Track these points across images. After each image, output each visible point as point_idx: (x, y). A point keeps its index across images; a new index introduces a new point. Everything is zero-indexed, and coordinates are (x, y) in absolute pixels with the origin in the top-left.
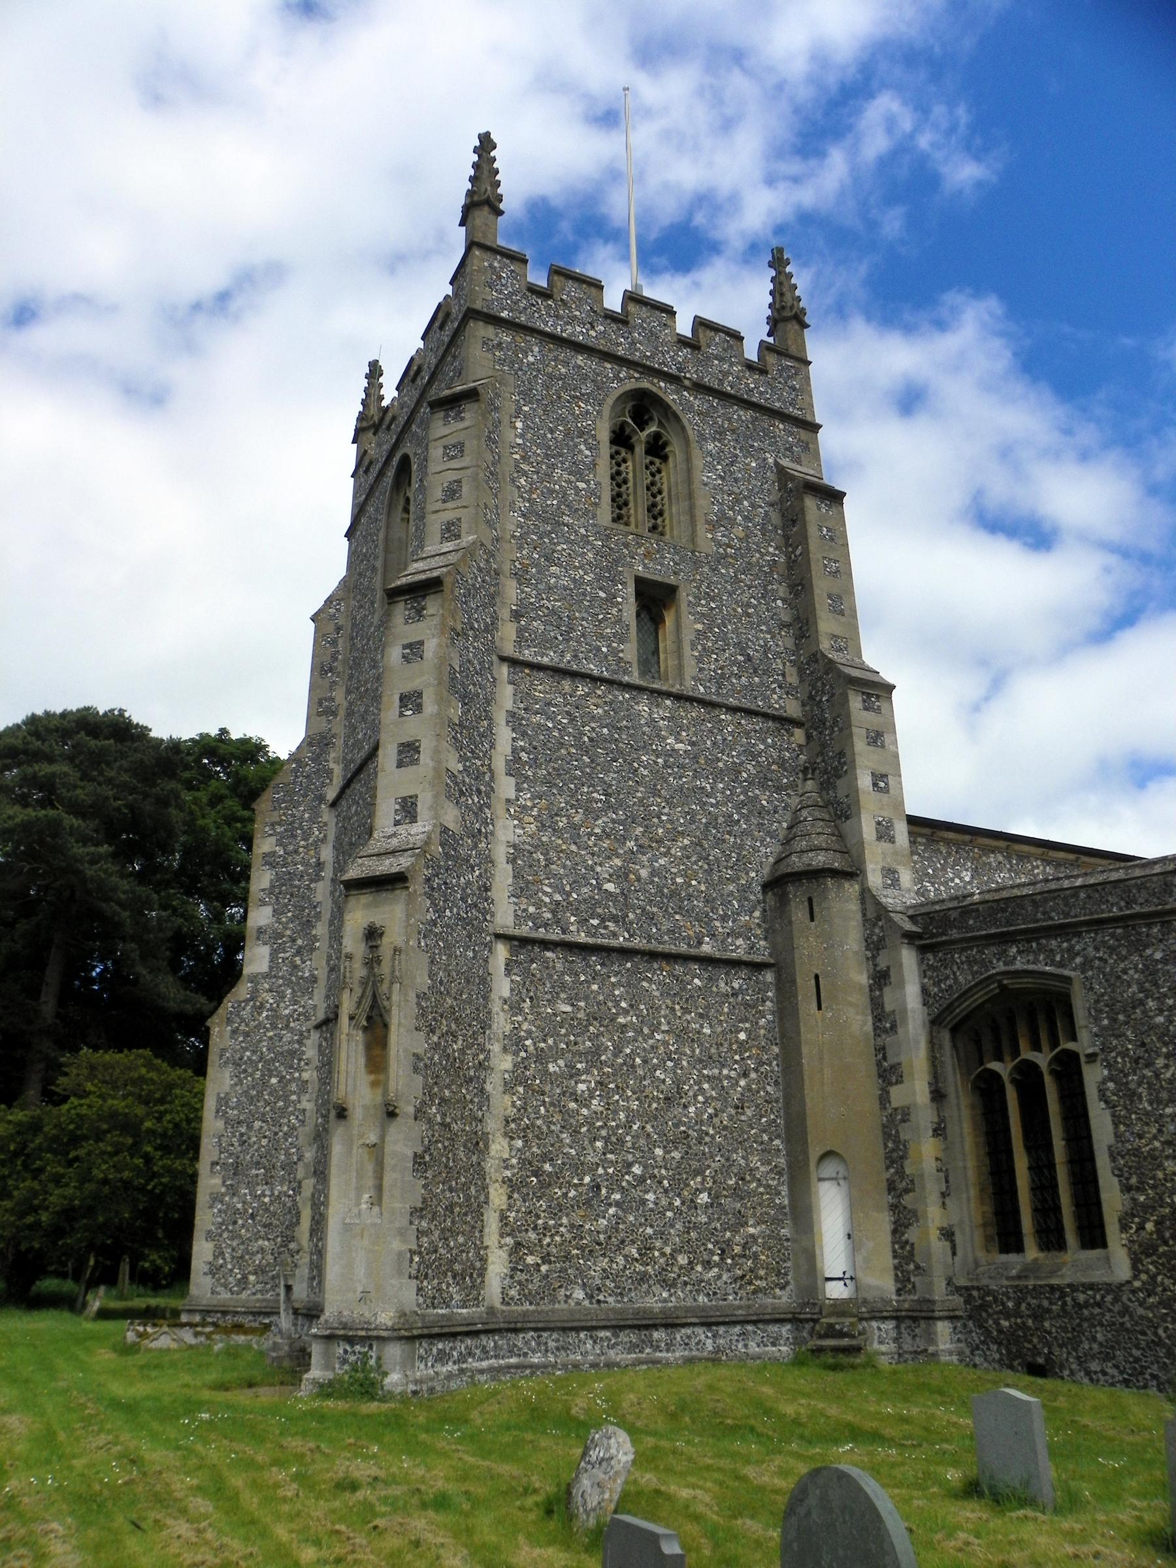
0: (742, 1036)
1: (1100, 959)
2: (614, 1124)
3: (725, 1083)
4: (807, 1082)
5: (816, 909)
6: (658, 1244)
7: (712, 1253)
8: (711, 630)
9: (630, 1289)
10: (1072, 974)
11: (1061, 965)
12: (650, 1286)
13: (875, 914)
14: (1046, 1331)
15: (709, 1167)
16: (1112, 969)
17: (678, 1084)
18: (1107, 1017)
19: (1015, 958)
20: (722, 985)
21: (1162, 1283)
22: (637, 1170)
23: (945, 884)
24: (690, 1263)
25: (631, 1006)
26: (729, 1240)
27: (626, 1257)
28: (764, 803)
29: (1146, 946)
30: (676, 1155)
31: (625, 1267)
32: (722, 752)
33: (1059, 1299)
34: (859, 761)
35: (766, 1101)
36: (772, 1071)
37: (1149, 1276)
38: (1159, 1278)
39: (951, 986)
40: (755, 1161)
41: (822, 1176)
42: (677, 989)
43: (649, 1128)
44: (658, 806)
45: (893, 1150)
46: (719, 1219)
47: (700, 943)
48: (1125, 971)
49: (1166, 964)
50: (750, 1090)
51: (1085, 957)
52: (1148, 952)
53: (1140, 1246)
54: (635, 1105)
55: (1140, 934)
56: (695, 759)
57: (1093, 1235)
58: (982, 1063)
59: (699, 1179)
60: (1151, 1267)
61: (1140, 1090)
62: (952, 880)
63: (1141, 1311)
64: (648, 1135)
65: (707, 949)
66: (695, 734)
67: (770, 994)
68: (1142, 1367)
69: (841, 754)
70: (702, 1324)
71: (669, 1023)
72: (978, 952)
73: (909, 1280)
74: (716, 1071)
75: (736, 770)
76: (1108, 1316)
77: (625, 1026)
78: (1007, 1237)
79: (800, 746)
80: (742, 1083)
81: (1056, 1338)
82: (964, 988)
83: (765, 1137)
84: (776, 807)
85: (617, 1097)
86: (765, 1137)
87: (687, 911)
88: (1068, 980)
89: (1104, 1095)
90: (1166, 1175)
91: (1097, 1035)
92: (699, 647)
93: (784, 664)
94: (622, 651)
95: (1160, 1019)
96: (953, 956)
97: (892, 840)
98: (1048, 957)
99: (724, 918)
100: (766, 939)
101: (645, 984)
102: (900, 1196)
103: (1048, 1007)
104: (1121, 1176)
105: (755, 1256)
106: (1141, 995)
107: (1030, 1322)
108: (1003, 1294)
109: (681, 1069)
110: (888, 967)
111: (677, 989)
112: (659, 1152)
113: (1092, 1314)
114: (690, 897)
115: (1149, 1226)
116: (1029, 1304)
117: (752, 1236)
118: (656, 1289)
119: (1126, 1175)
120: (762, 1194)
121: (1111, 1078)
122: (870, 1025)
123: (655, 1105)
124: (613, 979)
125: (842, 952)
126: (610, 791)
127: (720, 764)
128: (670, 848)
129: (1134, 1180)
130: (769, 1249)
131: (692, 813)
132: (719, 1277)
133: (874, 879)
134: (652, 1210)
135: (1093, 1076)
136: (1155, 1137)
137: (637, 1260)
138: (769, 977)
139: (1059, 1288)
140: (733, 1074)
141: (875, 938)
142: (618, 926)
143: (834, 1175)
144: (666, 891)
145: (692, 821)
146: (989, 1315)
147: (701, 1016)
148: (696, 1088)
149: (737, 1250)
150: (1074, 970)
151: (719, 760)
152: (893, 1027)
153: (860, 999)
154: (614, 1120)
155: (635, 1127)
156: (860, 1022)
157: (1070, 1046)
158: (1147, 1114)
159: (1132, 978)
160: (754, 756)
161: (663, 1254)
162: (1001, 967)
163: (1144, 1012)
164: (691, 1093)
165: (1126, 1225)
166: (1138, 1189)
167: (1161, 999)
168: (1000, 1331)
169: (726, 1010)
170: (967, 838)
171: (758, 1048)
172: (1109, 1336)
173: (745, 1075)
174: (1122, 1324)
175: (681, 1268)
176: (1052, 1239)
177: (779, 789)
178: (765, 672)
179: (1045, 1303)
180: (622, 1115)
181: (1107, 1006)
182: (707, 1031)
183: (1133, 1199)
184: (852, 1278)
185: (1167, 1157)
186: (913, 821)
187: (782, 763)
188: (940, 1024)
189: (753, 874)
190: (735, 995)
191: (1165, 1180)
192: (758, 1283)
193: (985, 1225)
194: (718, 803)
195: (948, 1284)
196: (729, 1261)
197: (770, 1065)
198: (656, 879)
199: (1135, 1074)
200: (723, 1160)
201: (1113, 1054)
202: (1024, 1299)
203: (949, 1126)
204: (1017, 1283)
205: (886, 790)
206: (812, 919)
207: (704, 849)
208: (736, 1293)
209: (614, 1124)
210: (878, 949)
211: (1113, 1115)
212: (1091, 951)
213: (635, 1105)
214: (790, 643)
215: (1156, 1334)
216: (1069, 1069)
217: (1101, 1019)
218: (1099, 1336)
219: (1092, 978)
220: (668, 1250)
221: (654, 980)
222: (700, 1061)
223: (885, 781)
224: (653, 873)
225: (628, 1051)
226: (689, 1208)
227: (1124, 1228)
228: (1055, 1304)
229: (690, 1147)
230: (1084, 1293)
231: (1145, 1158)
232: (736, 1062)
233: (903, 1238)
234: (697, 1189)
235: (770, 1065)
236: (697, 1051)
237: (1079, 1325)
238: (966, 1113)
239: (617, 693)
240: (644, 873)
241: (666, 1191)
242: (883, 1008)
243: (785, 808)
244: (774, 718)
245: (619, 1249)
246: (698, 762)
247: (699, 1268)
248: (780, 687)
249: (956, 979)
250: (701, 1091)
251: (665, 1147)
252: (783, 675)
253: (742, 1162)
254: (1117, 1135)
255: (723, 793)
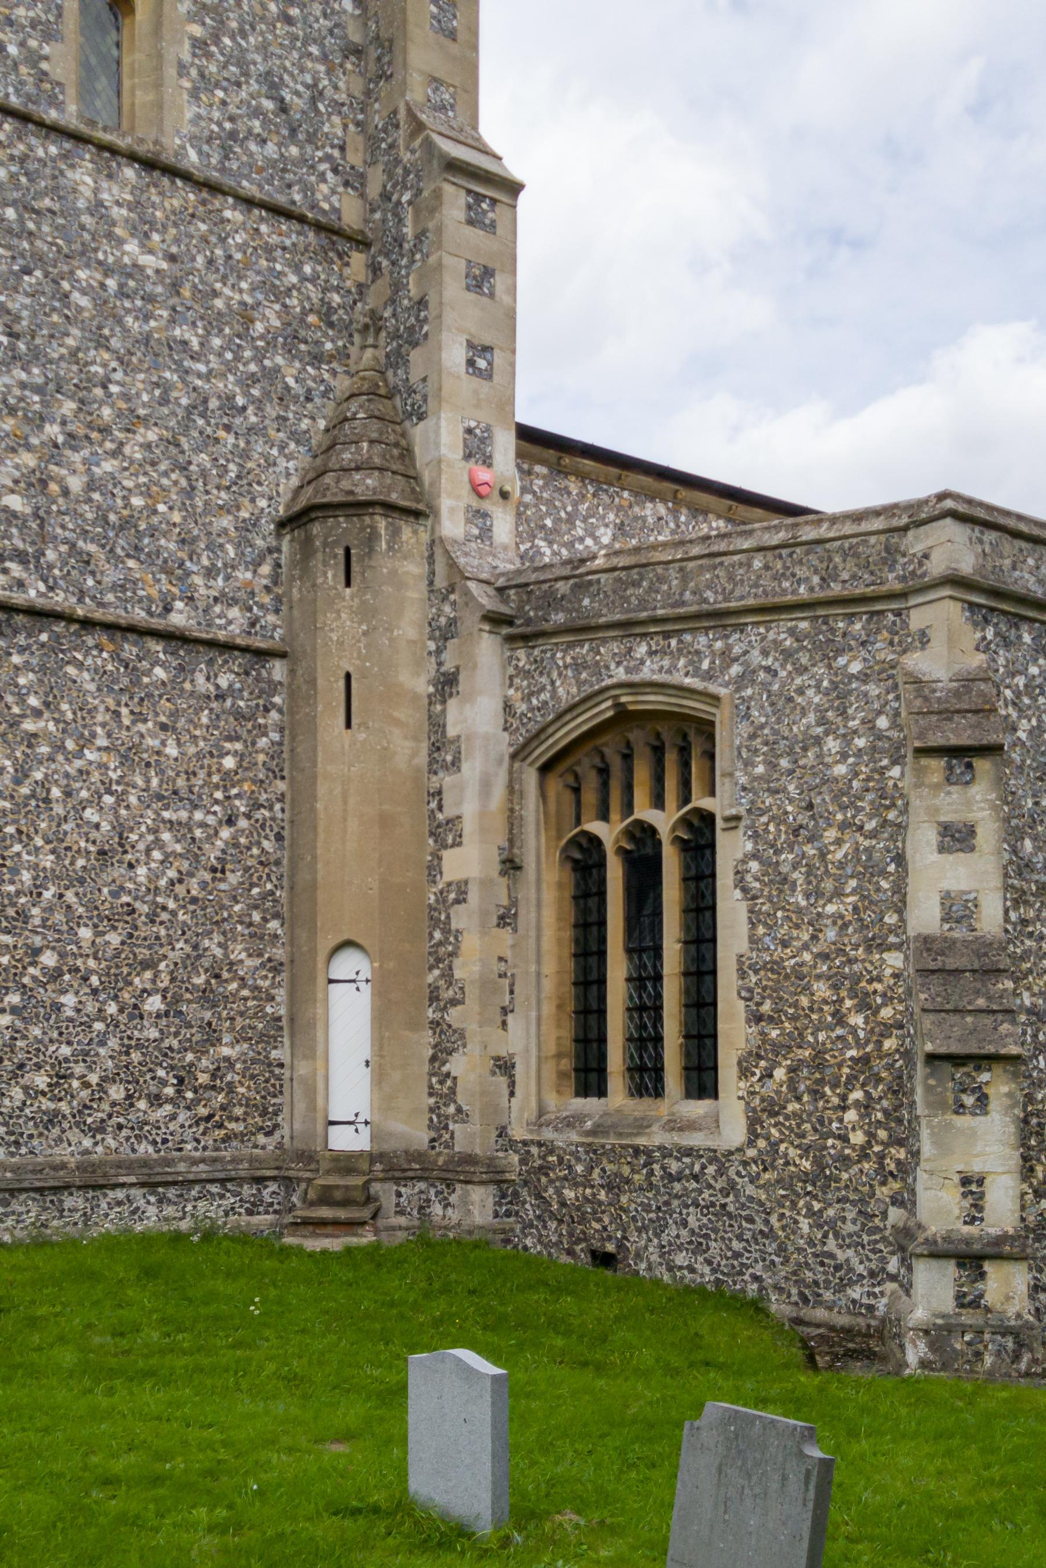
0: (229, 763)
1: (768, 669)
2: (11, 889)
3: (198, 833)
4: (321, 836)
5: (355, 567)
6: (79, 1069)
7: (164, 1083)
8: (217, 40)
9: (31, 1136)
10: (723, 692)
11: (709, 676)
12: (63, 1131)
13: (448, 581)
14: (621, 1208)
15: (165, 957)
16: (783, 685)
17: (121, 831)
18: (764, 762)
19: (642, 662)
20: (200, 679)
21: (786, 1155)
22: (49, 959)
23: (570, 545)
24: (129, 1097)
25: (47, 704)
26: (191, 1065)
27: (26, 1089)
28: (291, 381)
29: (840, 652)
30: (114, 939)
31: (24, 1103)
32: (224, 280)
33: (644, 1166)
34: (450, 317)
35: (261, 863)
36: (273, 819)
37: (770, 1144)
38: (783, 1147)
39: (546, 703)
40: (238, 952)
41: (332, 977)
42: (125, 681)
43: (70, 897)
44: (105, 365)
45: (440, 944)
46: (176, 1034)
47: (168, 609)
48: (801, 691)
49: (865, 682)
50: (236, 845)
51: (746, 664)
52: (842, 661)
53: (763, 1100)
54: (48, 861)
55: (833, 630)
56: (175, 287)
57: (702, 1081)
58: (578, 821)
59: (148, 975)
60: (773, 1131)
61: (795, 875)
62: (581, 540)
63: (750, 1190)
64: (69, 907)
65: (180, 618)
66: (177, 241)
67: (277, 700)
68: (742, 1264)
69: (422, 303)
70: (142, 1185)
71: (109, 735)
72: (591, 649)
73: (446, 1127)
74: (184, 815)
75: (246, 315)
76: (706, 1194)
77: (35, 735)
78: (589, 1078)
79: (360, 286)
80: (225, 833)
81: (634, 1218)
82: (564, 705)
83: (256, 917)
84: (309, 391)
85: (17, 848)
86: (256, 917)
87: (149, 555)
88: (715, 699)
89: (742, 880)
90: (813, 1002)
91: (744, 789)
92: (194, 72)
93: (345, 127)
94: (46, 58)
95: (841, 770)
96: (553, 656)
97: (488, 461)
98: (691, 662)
99: (210, 573)
100: (277, 611)
101: (71, 670)
102: (444, 1009)
103: (679, 738)
104: (749, 999)
105: (231, 1088)
106: (819, 730)
107: (602, 1195)
108: (571, 1154)
109: (128, 807)
110: (458, 668)
111: (125, 681)
112: (85, 933)
113: (685, 1189)
114: (153, 532)
115: (780, 1074)
116: (603, 1170)
117: (227, 1059)
118: (74, 1135)
119: (757, 998)
120: (246, 999)
121: (755, 856)
122: (439, 752)
123: (81, 862)
124: (16, 659)
125: (390, 639)
126: (17, 328)
127: (219, 303)
128: (121, 444)
129: (767, 1007)
130: (253, 1077)
131: (167, 388)
132: (173, 1117)
133: (452, 524)
134: (70, 1020)
135: (731, 849)
136: (806, 947)
137: (43, 1093)
138: (278, 670)
139: (648, 1152)
140: (211, 820)
141: (443, 620)
142: (27, 569)
143: (353, 977)
144: (112, 517)
145: (164, 401)
146: (551, 1181)
147: (164, 727)
148: (150, 838)
149: (203, 1078)
150: (726, 685)
151: (215, 294)
152: (456, 763)
153: (410, 715)
154: (12, 882)
155: (47, 895)
156: (408, 751)
157: (705, 803)
158: (799, 911)
159: (810, 703)
160: (279, 294)
161: (86, 1085)
162: (620, 674)
163: (820, 756)
164: (141, 846)
165: (747, 1069)
166: (771, 1019)
167: (847, 738)
168: (563, 1204)
169: (205, 720)
170: (614, 471)
171: (254, 782)
172: (705, 1220)
173: (230, 822)
174: (724, 1206)
175: (114, 1104)
176: (647, 1079)
177: (317, 359)
178: (311, 138)
179: (626, 1170)
180: (26, 876)
181: (766, 743)
182: (172, 750)
183: (762, 1033)
184: (366, 1123)
185: (819, 977)
186: (527, 435)
187: (326, 313)
188: (524, 760)
189: (263, 503)
190: (220, 697)
191: (811, 1009)
192: (232, 1126)
193: (559, 1056)
194: (210, 371)
195: (500, 1136)
196: (189, 1095)
197: (271, 808)
198: (96, 496)
199: (792, 851)
200: (188, 949)
201: (764, 819)
202: (598, 1162)
203: (522, 912)
204: (589, 1140)
205: (487, 375)
206: (348, 584)
207: (183, 452)
208: (198, 1141)
209: (11, 889)
210: (446, 639)
211: (751, 911)
212: (756, 657)
213: (48, 861)
214: (358, 87)
215: (767, 1222)
216: (699, 837)
217: (754, 765)
218: (691, 1220)
219: (751, 698)
220: (94, 1079)
221: (88, 666)
222: (160, 797)
223: (488, 358)
224: (91, 486)
225: (38, 776)
226: (131, 1017)
227: (745, 1072)
228: (638, 1172)
229: (136, 928)
230: (678, 1159)
231: (787, 977)
232: (217, 802)
233: (445, 1069)
234: (144, 991)
235: (271, 808)
236: (155, 782)
237: (667, 1203)
238: (549, 895)
239: (33, 141)
240: (76, 484)
241: (95, 992)
242: (444, 732)
243: (324, 395)
244: (319, 227)
245: (16, 1076)
246: (178, 293)
247: (142, 1105)
248: (335, 171)
249: (554, 690)
250: (158, 843)
251: (95, 926)
252: (342, 148)
253: (218, 952)
254: (753, 940)
255: (220, 355)
